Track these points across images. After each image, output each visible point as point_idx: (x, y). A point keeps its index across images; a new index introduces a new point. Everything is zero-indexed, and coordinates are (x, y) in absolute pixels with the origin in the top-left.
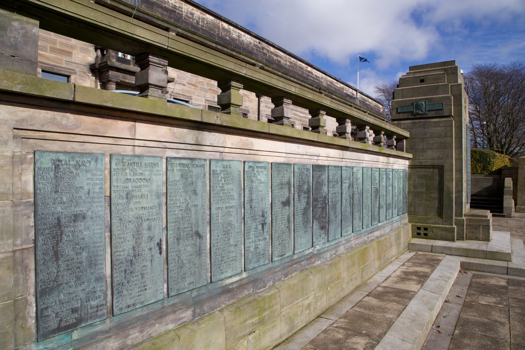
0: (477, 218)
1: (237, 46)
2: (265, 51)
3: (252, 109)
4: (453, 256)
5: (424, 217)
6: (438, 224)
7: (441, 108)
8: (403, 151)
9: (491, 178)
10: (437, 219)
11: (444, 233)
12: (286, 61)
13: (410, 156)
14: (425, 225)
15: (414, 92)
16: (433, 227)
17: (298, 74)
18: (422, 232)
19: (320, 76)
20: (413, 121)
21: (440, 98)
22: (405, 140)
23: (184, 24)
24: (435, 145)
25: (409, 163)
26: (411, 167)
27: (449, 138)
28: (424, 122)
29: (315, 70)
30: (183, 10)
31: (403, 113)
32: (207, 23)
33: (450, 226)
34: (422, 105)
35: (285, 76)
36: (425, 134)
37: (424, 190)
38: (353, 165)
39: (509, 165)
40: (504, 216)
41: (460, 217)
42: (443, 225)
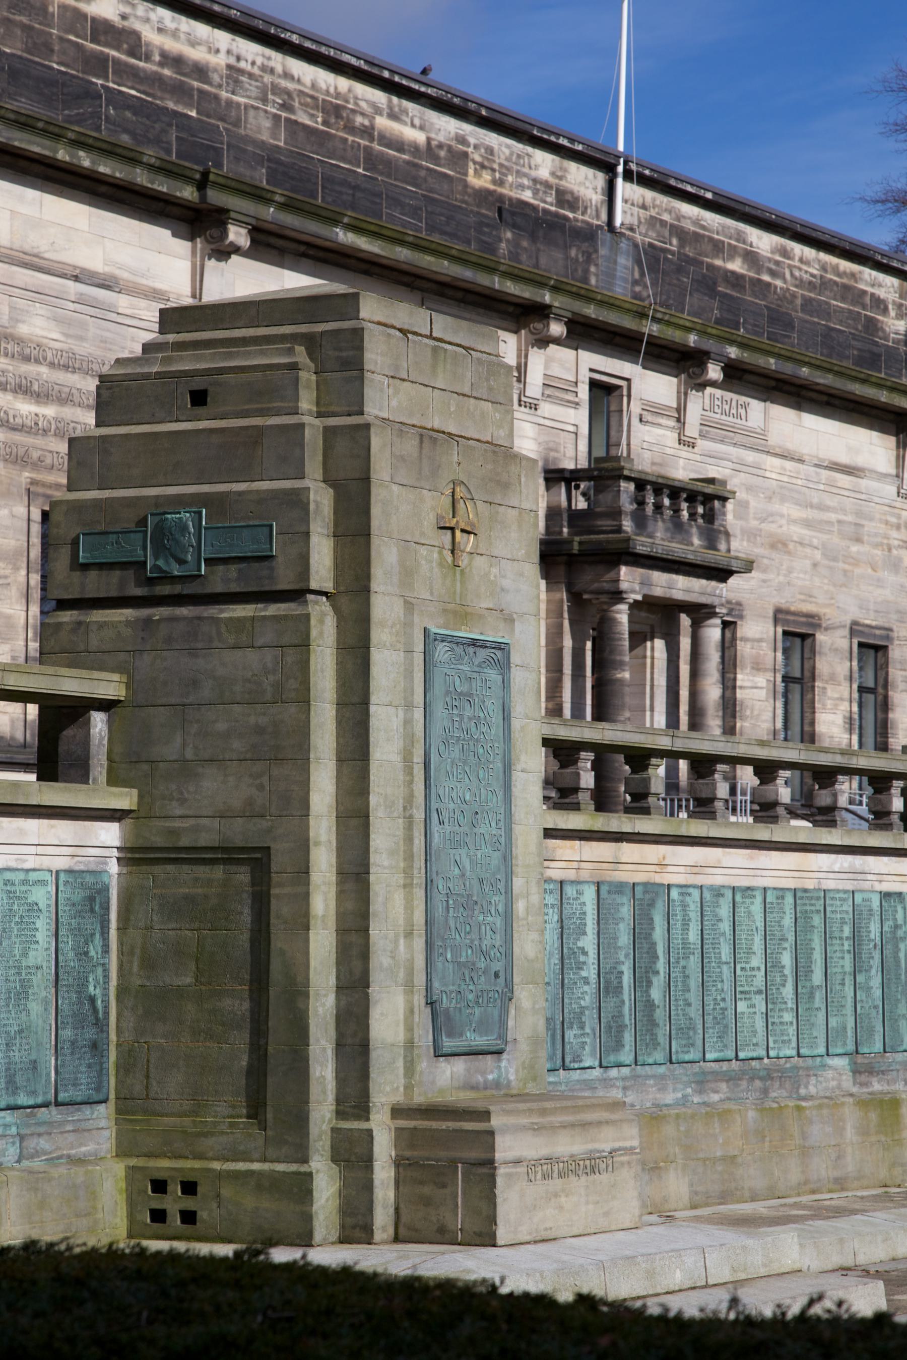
0: (444, 1125)
5: (187, 1121)
13: (124, 799)
15: (162, 456)
16: (220, 1175)
18: (174, 1202)
20: (144, 612)
24: (236, 744)
25: (124, 838)
26: (134, 856)
27: (293, 709)
31: (101, 566)
33: (293, 1167)
34: (184, 528)
36: (195, 683)
37: (189, 980)
42: (264, 1160)
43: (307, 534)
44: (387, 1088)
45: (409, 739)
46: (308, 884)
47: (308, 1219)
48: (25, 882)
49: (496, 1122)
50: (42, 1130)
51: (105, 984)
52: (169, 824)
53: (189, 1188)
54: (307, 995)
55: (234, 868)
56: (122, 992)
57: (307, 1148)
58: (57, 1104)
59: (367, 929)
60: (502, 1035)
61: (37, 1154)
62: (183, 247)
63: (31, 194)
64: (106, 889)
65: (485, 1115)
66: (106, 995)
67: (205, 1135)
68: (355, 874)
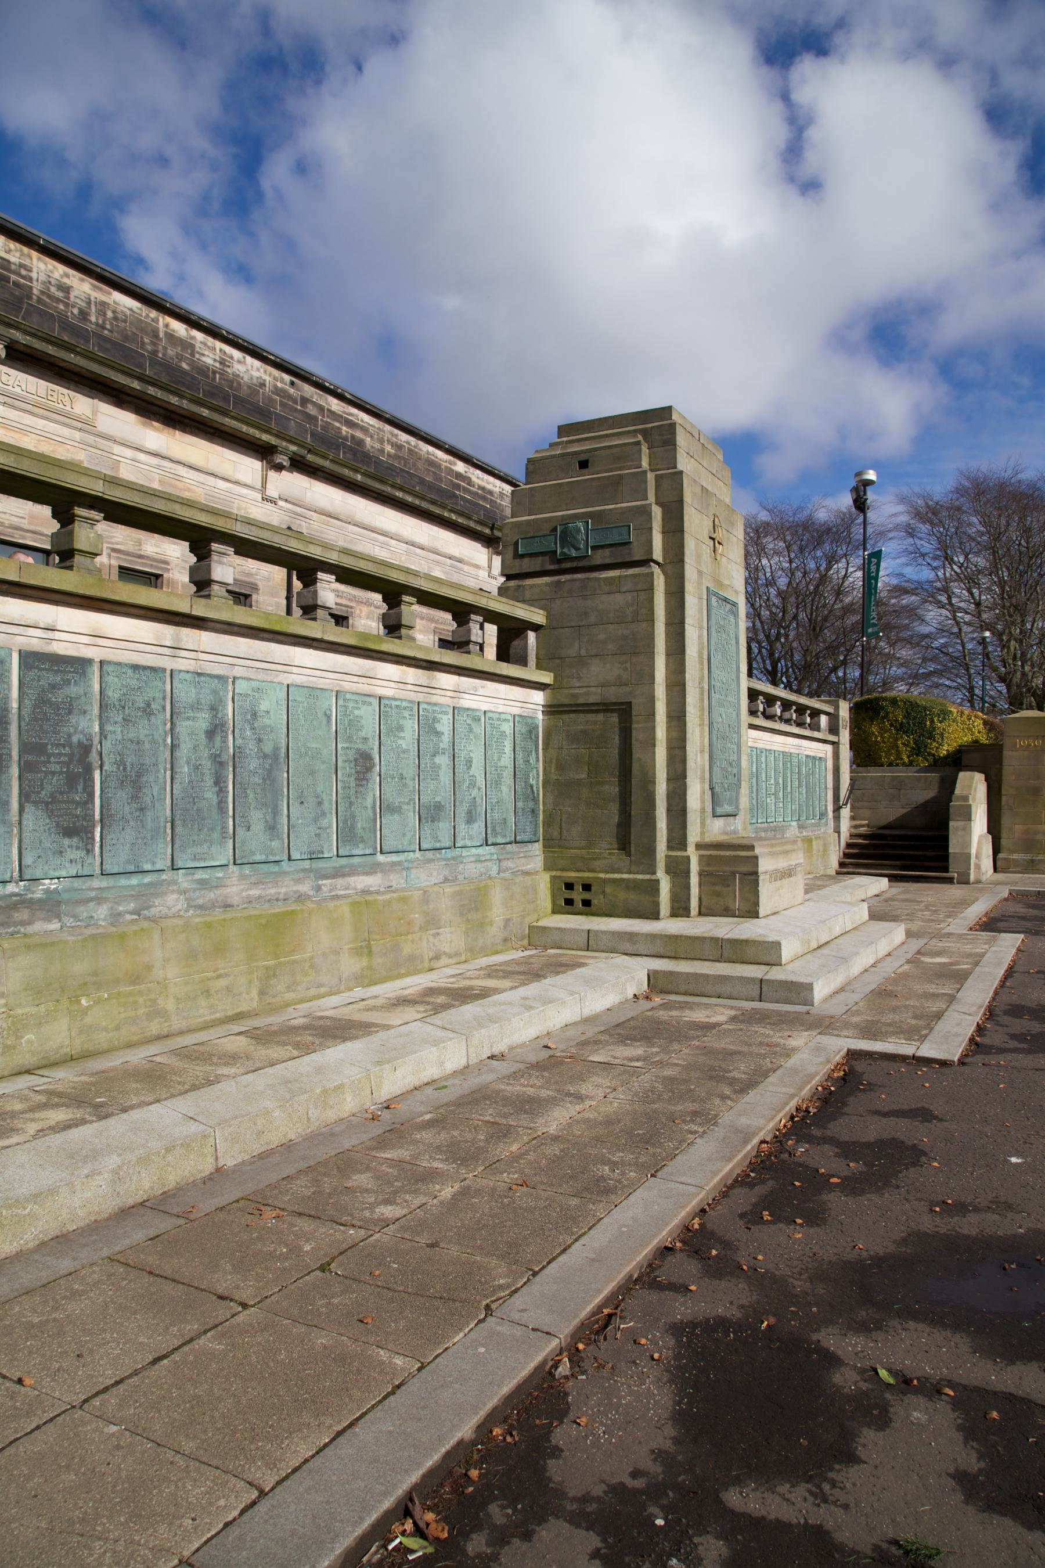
0: (728, 853)
1: (215, 391)
2: (311, 410)
3: (268, 579)
4: (639, 959)
6: (620, 872)
7: (625, 539)
8: (526, 665)
9: (934, 776)
10: (618, 858)
11: (633, 897)
12: (381, 441)
13: (547, 678)
14: (586, 875)
16: (604, 880)
17: (422, 482)
18: (578, 895)
19: (497, 490)
21: (623, 512)
22: (531, 636)
23: (35, 318)
24: (611, 646)
25: (546, 700)
26: (552, 710)
27: (644, 625)
28: (582, 580)
29: (478, 472)
30: (34, 275)
32: (115, 318)
33: (647, 877)
34: (578, 531)
35: (377, 486)
36: (586, 614)
37: (584, 776)
38: (238, 672)
39: (983, 739)
40: (950, 881)
41: (680, 850)
43: (651, 528)
44: (693, 836)
45: (701, 644)
46: (654, 721)
47: (657, 904)
48: (499, 719)
49: (757, 851)
50: (508, 856)
51: (537, 779)
52: (572, 691)
53: (587, 887)
54: (654, 783)
55: (609, 714)
56: (545, 783)
57: (655, 866)
58: (516, 842)
59: (685, 747)
60: (737, 807)
61: (507, 869)
62: (485, 550)
63: (435, 528)
64: (537, 727)
65: (752, 848)
66: (538, 784)
67: (594, 859)
68: (678, 717)
